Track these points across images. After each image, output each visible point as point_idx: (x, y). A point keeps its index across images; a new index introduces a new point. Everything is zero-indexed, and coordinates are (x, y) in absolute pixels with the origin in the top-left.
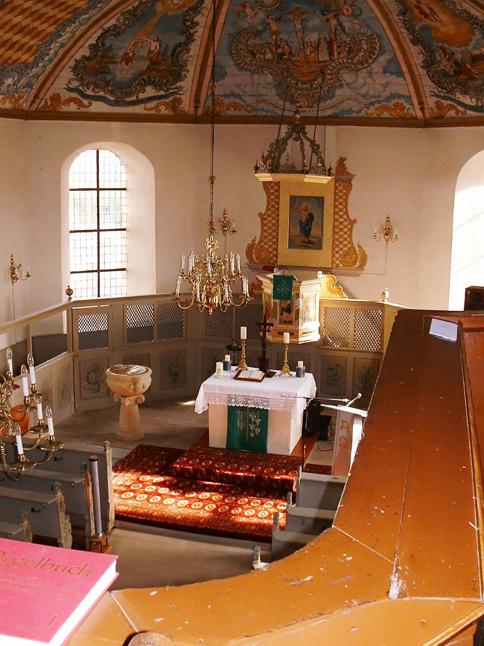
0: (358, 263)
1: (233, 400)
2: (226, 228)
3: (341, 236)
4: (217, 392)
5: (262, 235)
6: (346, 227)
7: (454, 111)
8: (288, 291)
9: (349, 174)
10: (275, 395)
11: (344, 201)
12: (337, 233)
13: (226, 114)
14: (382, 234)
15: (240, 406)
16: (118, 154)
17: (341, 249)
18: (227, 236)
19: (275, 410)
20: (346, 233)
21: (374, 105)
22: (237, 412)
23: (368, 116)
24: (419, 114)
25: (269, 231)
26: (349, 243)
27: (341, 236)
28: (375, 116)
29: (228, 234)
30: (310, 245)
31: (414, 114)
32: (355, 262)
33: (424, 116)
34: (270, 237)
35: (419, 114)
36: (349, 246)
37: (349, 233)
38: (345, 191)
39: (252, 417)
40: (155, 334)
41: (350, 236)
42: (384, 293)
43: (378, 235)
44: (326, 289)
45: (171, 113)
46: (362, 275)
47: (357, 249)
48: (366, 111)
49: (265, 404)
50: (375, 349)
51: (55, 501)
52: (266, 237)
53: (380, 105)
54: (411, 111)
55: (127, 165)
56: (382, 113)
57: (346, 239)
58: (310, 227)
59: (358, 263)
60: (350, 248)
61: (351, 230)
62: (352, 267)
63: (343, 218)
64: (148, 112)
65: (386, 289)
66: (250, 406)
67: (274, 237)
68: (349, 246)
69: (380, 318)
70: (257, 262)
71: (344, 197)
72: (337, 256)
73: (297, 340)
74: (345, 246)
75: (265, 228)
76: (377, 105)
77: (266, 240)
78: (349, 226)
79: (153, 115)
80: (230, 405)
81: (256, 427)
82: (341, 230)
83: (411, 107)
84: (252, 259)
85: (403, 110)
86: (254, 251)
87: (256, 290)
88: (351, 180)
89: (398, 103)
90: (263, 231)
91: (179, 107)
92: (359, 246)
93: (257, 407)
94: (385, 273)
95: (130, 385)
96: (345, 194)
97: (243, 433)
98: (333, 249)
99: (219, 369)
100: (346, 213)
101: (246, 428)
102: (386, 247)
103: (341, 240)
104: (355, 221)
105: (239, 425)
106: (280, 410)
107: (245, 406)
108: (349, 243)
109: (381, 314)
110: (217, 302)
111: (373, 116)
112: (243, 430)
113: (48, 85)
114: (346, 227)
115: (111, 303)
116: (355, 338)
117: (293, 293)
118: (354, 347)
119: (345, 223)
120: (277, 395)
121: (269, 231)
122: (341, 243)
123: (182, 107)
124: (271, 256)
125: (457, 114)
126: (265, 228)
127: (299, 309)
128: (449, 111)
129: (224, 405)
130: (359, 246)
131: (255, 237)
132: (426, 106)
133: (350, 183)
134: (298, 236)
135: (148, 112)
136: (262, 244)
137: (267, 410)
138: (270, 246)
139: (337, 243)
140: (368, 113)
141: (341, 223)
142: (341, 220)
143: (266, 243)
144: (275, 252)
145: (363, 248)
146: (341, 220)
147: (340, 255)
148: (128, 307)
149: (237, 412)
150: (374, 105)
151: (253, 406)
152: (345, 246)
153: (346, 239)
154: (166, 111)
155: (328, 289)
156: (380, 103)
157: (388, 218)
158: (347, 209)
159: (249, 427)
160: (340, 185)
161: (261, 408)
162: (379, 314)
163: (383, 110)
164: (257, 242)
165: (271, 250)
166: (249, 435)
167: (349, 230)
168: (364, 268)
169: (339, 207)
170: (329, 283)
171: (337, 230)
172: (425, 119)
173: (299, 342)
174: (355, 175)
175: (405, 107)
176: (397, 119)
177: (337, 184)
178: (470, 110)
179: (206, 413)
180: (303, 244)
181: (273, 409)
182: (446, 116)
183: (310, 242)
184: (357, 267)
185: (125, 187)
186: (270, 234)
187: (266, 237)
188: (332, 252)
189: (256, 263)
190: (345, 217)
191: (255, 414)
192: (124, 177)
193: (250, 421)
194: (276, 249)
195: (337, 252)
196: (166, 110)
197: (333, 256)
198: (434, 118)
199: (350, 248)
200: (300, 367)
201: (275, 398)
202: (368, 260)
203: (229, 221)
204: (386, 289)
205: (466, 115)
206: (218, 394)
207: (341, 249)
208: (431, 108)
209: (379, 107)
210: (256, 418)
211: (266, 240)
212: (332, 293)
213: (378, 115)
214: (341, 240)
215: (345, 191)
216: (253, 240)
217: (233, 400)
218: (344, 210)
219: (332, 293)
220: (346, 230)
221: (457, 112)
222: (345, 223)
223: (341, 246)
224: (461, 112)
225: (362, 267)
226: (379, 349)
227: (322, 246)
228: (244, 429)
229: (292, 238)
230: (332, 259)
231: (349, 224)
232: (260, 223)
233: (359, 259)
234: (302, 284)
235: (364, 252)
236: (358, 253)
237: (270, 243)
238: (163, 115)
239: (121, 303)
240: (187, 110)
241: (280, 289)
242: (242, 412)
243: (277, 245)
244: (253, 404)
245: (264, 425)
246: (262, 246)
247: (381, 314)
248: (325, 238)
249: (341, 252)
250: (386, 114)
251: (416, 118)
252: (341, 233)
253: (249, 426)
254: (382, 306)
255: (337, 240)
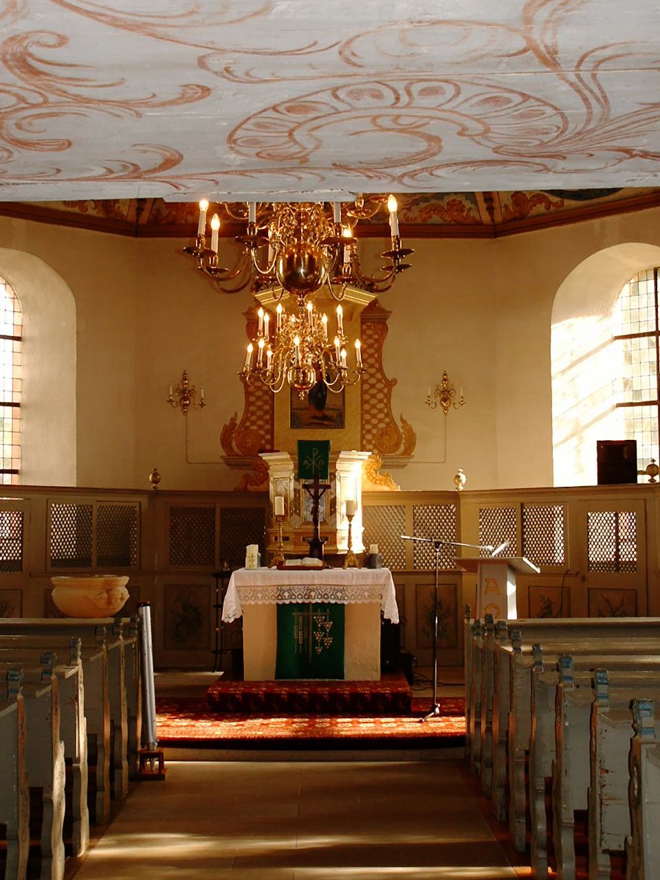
0: (402, 447)
1: (286, 594)
2: (188, 402)
3: (374, 406)
4: (259, 583)
5: (247, 410)
6: (380, 391)
7: (544, 204)
8: (323, 464)
9: (383, 311)
10: (355, 578)
11: (376, 352)
12: (367, 402)
13: (186, 221)
14: (439, 399)
15: (297, 603)
16: (11, 278)
17: (375, 426)
18: (188, 414)
19: (356, 603)
20: (380, 401)
21: (417, 205)
22: (293, 614)
23: (410, 222)
24: (486, 218)
25: (259, 403)
26: (387, 415)
27: (374, 406)
28: (419, 221)
29: (190, 410)
30: (326, 423)
31: (478, 218)
32: (397, 445)
33: (493, 220)
34: (260, 413)
35: (486, 218)
36: (387, 420)
37: (385, 401)
38: (376, 337)
39: (319, 618)
40: (94, 563)
41: (388, 405)
42: (459, 477)
43: (432, 399)
44: (366, 476)
45: (101, 215)
46: (409, 464)
47: (400, 424)
48: (405, 215)
49: (339, 594)
50: (448, 567)
51: (117, 647)
52: (253, 413)
53: (427, 204)
54: (472, 214)
55: (24, 299)
56: (431, 217)
57: (381, 411)
58: (324, 393)
59: (402, 447)
60: (388, 425)
61: (388, 396)
62: (393, 454)
63: (376, 378)
64: (69, 209)
65: (460, 470)
66: (314, 602)
67: (266, 412)
68: (387, 420)
69: (454, 517)
70: (240, 454)
71: (376, 346)
72: (369, 437)
73: (335, 548)
74: (381, 421)
75: (252, 399)
76: (423, 205)
77: (253, 418)
78: (385, 390)
79: (75, 214)
80: (280, 602)
81: (325, 636)
82: (373, 396)
83: (473, 206)
84: (232, 449)
85: (462, 211)
86: (233, 436)
87: (251, 485)
88: (386, 319)
89: (454, 200)
90: (249, 404)
91: (114, 207)
92: (403, 421)
93: (326, 601)
94: (445, 459)
95: (102, 593)
96: (377, 341)
97: (303, 650)
98: (363, 426)
99: (252, 556)
100: (380, 370)
101: (308, 639)
102: (445, 420)
103: (374, 411)
104: (395, 382)
105: (298, 635)
106: (363, 603)
107: (306, 601)
108: (387, 415)
109: (454, 511)
110: (312, 382)
111: (416, 222)
112: (303, 645)
113: (72, 82)
114: (380, 391)
115: (28, 496)
116: (415, 552)
117: (330, 471)
118: (415, 568)
119: (380, 386)
120: (358, 578)
121: (259, 403)
122: (374, 416)
123: (119, 207)
124: (263, 442)
125: (549, 208)
126: (252, 399)
127: (336, 497)
128: (535, 205)
129: (270, 604)
130: (403, 421)
131: (236, 414)
132: (496, 205)
133: (384, 324)
134: (305, 409)
135: (69, 209)
136: (248, 424)
137: (343, 604)
138: (261, 427)
139: (367, 417)
140: (408, 217)
141: (373, 386)
142: (373, 381)
143: (253, 423)
144: (268, 437)
145: (409, 423)
146: (373, 381)
147: (374, 435)
148: (53, 505)
149: (293, 614)
150: (417, 205)
151: (319, 601)
152: (381, 421)
153: (381, 411)
154: (96, 211)
155: (368, 477)
156: (429, 201)
157: (445, 375)
158: (381, 364)
159: (314, 637)
160: (369, 328)
161: (333, 602)
162: (452, 512)
163: (432, 212)
164: (238, 422)
165: (262, 432)
166: (314, 650)
167: (386, 395)
168: (413, 454)
169: (368, 360)
170: (369, 467)
171: (366, 397)
172: (494, 225)
173: (337, 550)
174: (390, 312)
175: (464, 206)
176: (453, 225)
177: (365, 327)
178: (569, 198)
179: (239, 621)
180: (313, 420)
181: (353, 602)
182: (529, 215)
183: (326, 418)
184: (400, 452)
185: (19, 335)
186: (260, 408)
187: (253, 413)
188: (361, 432)
189: (237, 455)
190: (379, 376)
191: (324, 614)
192: (18, 318)
193: (315, 628)
194: (271, 432)
195: (369, 431)
196: (94, 209)
197: (363, 437)
198: (510, 221)
199: (388, 425)
200: (374, 553)
201: (354, 583)
202: (417, 441)
203: (193, 390)
204: (460, 470)
205: (562, 208)
206: (261, 586)
207: (375, 426)
208: (506, 206)
209: (425, 208)
210: (325, 620)
211: (253, 418)
212: (375, 483)
213: (424, 220)
214: (374, 411)
215: (376, 337)
216: (232, 419)
217: (286, 594)
218: (377, 365)
219: (375, 483)
220: (380, 396)
221: (549, 204)
222: (380, 386)
223: (374, 421)
224: (555, 204)
225: (408, 452)
226: (455, 568)
227: (344, 423)
228: (305, 641)
229: (296, 411)
230: (362, 442)
231: (385, 387)
232: (243, 391)
233: (403, 441)
234: (341, 456)
235: (411, 429)
236: (401, 430)
237: (260, 423)
238: (90, 217)
239: (43, 496)
240: (125, 213)
241: (310, 462)
242: (301, 613)
243: (273, 425)
244: (320, 597)
245: (338, 632)
246: (247, 428)
247: (454, 511)
248: (348, 410)
249: (374, 431)
250: (436, 219)
251: (480, 223)
252: (373, 401)
253: (313, 635)
254: (455, 497)
255: (367, 412)
